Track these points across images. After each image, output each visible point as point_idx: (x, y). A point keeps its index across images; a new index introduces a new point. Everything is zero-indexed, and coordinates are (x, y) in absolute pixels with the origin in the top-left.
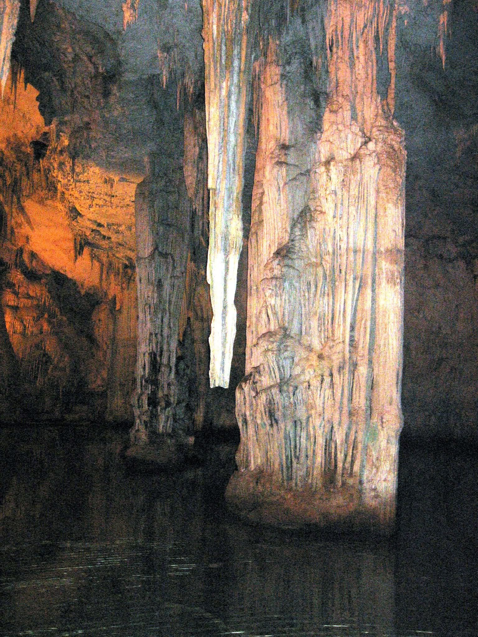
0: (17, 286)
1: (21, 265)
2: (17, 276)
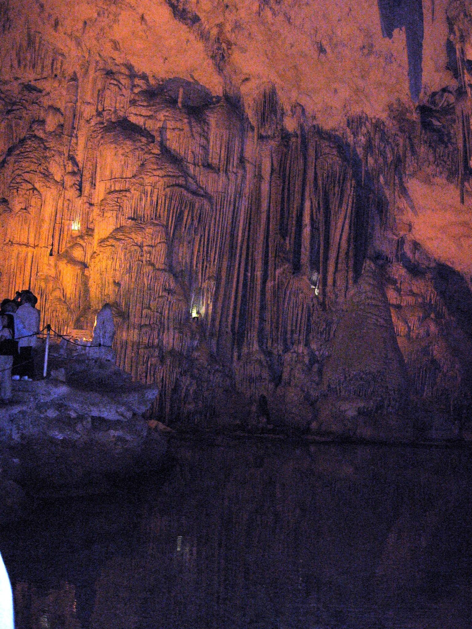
0: (399, 282)
1: (402, 258)
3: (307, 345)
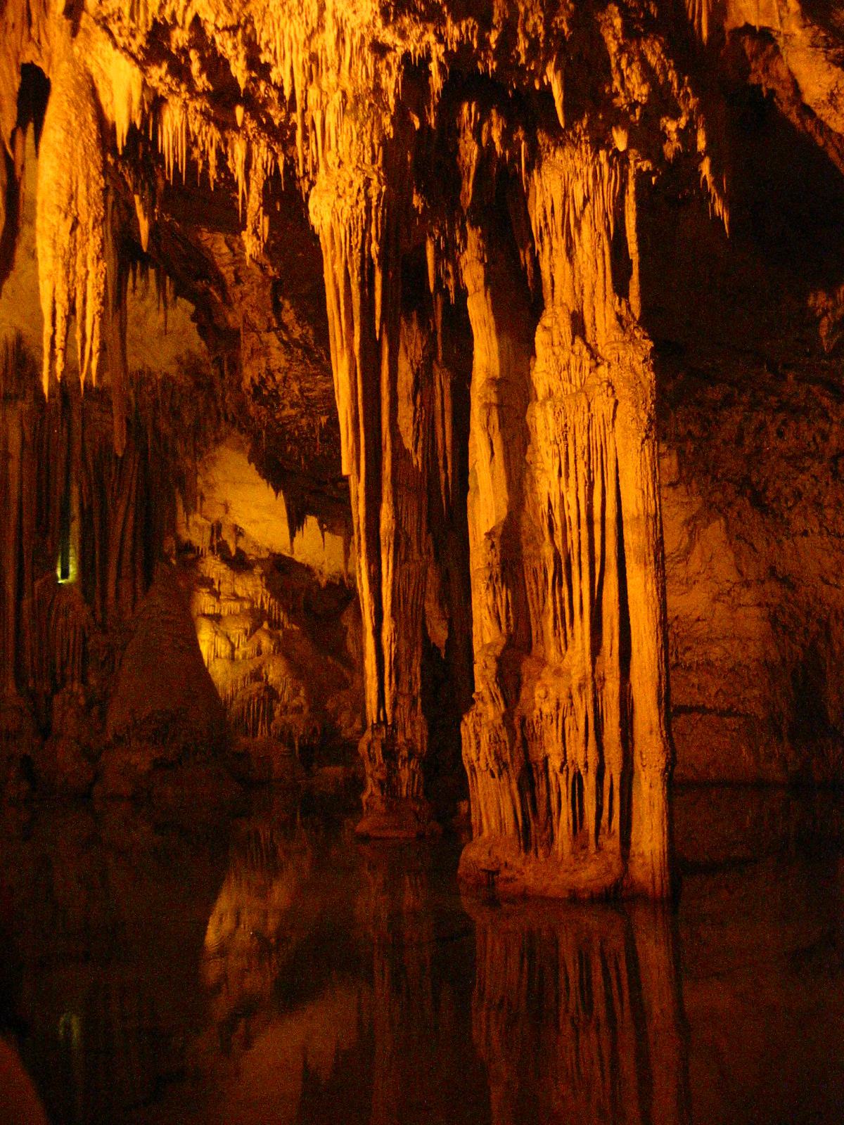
0: (217, 583)
2: (213, 567)
3: (84, 681)
